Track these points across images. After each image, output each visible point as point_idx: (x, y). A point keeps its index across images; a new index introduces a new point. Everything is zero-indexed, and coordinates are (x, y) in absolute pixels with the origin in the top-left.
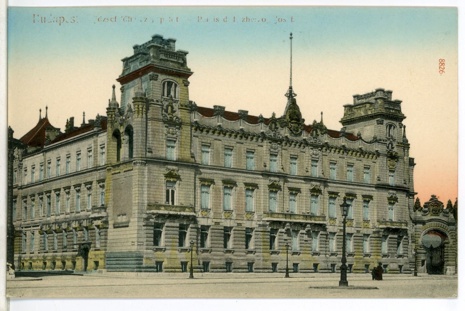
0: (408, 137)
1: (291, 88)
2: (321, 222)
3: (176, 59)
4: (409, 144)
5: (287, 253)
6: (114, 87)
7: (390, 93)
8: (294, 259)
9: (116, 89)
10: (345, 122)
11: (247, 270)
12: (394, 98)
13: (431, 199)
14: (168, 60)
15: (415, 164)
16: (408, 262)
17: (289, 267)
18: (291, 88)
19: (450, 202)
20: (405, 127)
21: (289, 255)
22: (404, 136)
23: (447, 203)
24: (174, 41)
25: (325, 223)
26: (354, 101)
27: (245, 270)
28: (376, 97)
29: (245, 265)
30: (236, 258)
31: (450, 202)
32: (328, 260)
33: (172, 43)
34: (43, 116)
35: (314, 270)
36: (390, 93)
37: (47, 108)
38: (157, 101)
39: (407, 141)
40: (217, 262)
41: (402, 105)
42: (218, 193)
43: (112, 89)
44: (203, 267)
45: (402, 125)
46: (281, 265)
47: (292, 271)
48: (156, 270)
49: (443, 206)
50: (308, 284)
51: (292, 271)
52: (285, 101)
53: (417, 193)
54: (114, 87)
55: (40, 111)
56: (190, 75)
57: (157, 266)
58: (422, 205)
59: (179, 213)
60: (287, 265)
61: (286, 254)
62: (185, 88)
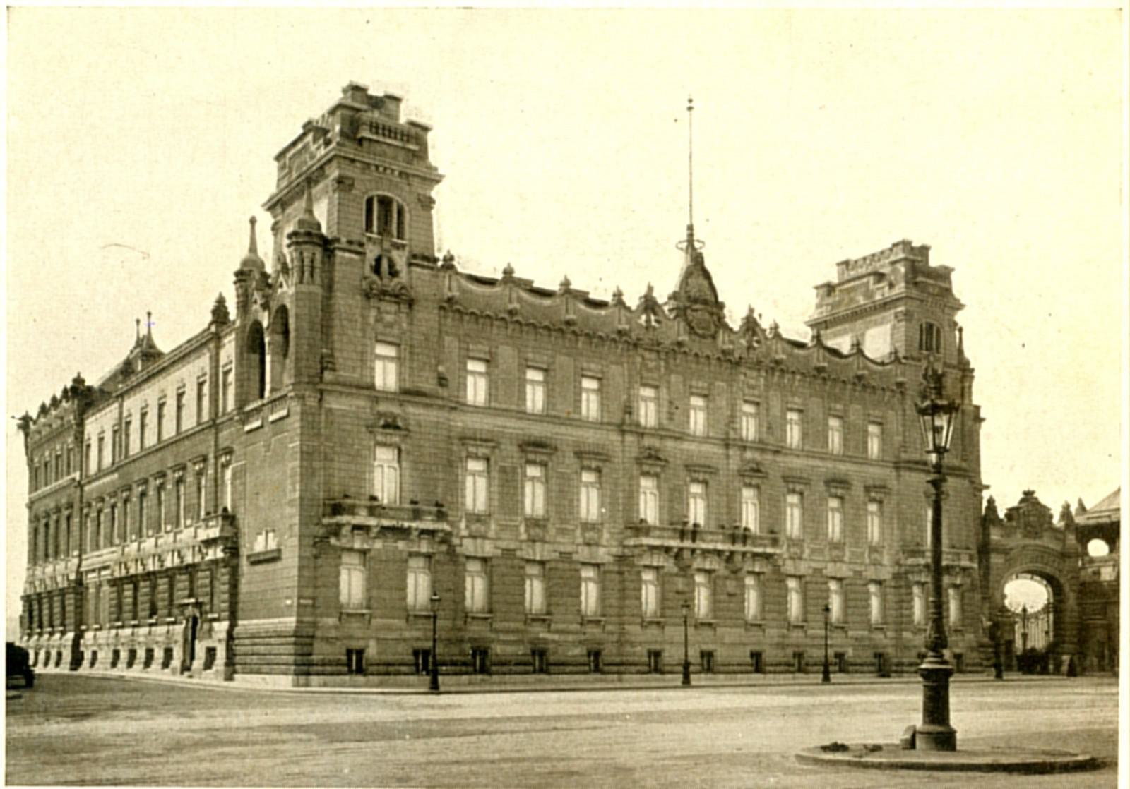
0: (968, 354)
1: (690, 228)
2: (769, 550)
3: (402, 140)
4: (973, 370)
5: (686, 625)
6: (253, 221)
7: (924, 250)
8: (700, 641)
9: (257, 226)
10: (819, 326)
11: (750, 668)
12: (934, 261)
13: (1022, 501)
14: (377, 142)
15: (983, 420)
16: (974, 644)
17: (691, 659)
18: (690, 228)
19: (1067, 508)
20: (961, 330)
21: (691, 630)
22: (960, 351)
23: (1060, 509)
24: (397, 100)
25: (778, 551)
26: (841, 274)
27: (582, 668)
28: (893, 258)
29: (582, 656)
30: (556, 637)
31: (1067, 508)
32: (787, 641)
33: (391, 105)
34: (143, 332)
35: (752, 665)
36: (924, 250)
37: (149, 314)
38: (350, 242)
39: (968, 363)
40: (510, 649)
41: (953, 276)
42: (510, 477)
43: (249, 226)
44: (413, 662)
45: (955, 324)
46: (672, 655)
47: (698, 668)
48: (346, 669)
49: (1051, 517)
50: (812, 737)
51: (837, 668)
52: (678, 263)
53: (987, 487)
54: (253, 221)
55: (138, 322)
56: (438, 182)
57: (350, 659)
58: (1001, 514)
59: (406, 524)
60: (686, 655)
61: (683, 628)
62: (422, 213)
